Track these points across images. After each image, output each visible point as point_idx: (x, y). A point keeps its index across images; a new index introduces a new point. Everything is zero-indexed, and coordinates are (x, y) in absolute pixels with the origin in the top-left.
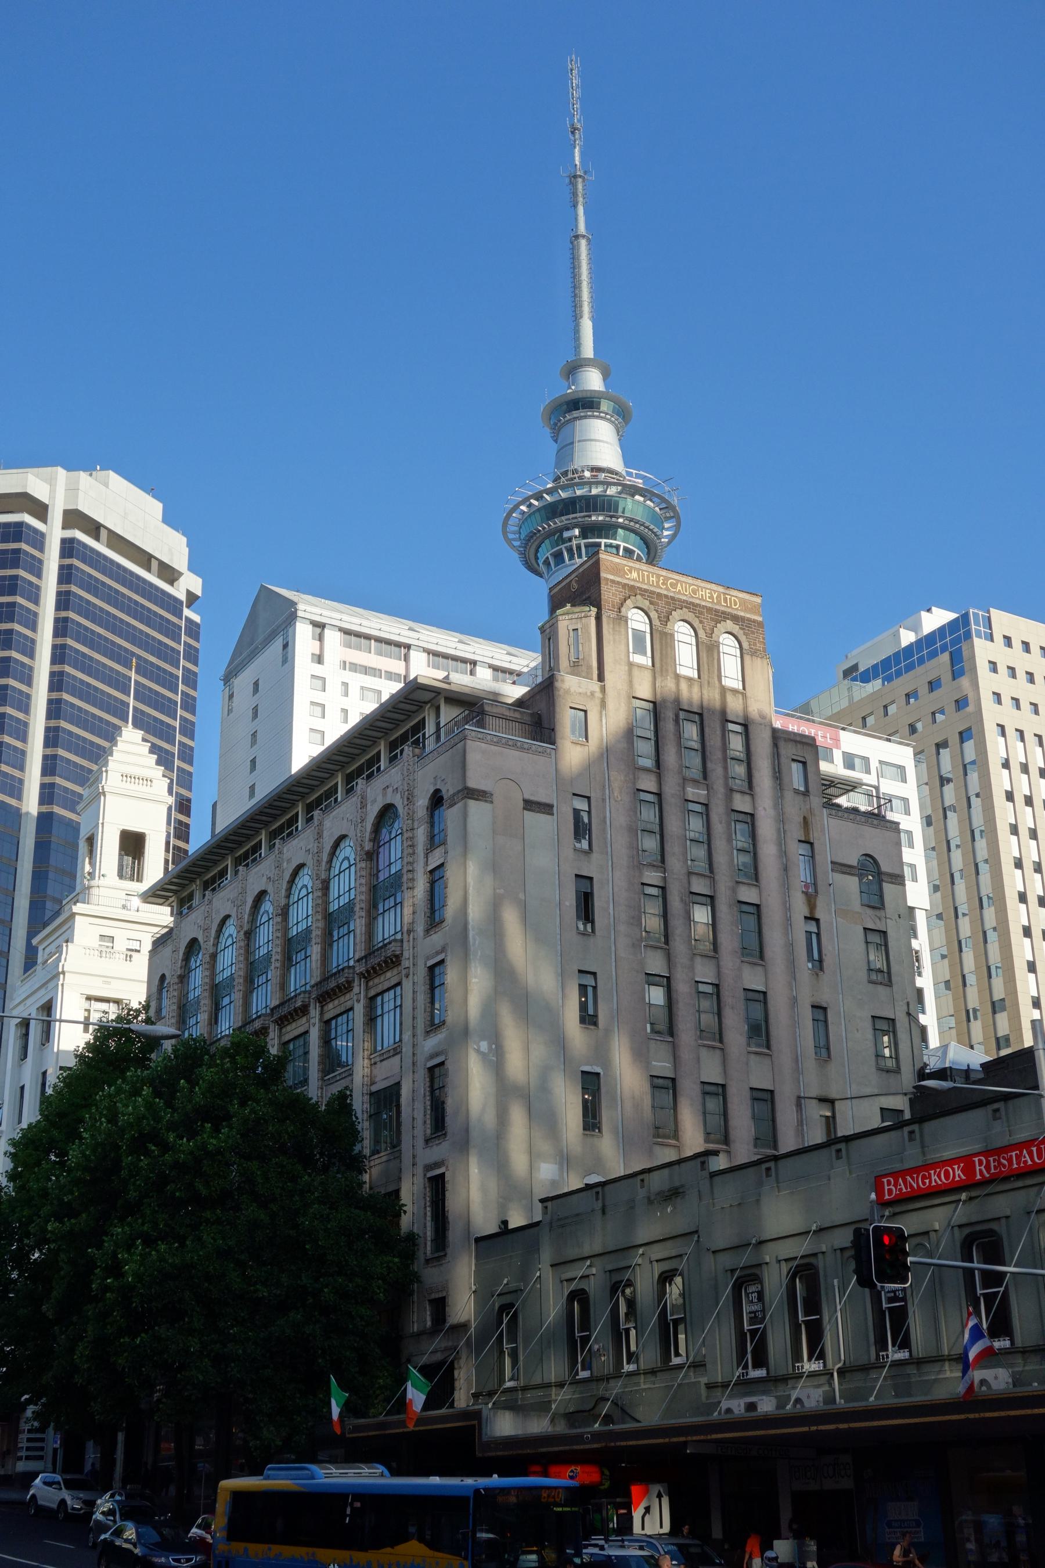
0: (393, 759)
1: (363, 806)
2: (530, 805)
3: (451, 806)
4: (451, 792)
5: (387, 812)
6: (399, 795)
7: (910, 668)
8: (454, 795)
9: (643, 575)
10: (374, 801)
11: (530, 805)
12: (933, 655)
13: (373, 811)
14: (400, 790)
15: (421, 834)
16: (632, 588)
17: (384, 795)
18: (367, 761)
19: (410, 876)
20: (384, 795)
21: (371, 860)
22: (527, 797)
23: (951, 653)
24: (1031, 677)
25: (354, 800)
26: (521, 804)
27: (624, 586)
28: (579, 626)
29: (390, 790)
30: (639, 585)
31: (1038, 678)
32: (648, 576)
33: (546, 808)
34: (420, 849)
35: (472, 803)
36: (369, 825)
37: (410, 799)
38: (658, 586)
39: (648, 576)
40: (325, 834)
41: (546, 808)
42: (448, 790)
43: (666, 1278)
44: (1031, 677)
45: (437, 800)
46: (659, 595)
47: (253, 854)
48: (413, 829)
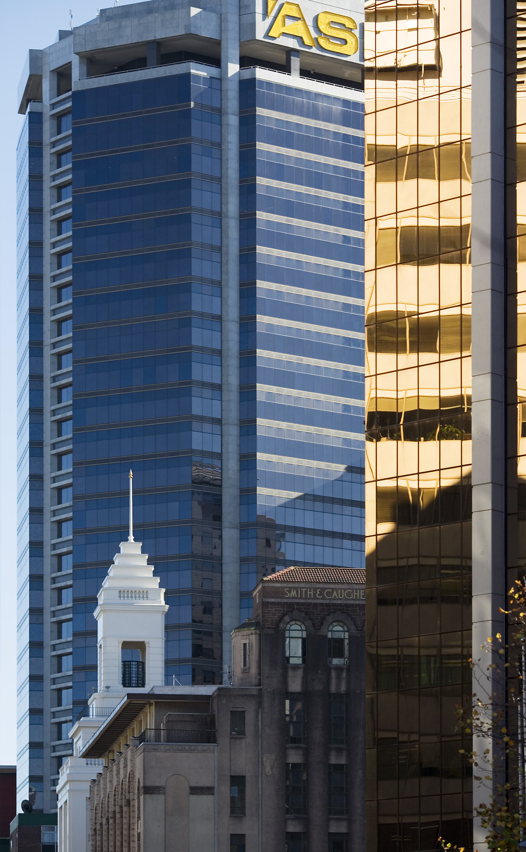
2: (195, 790)
9: (301, 592)
11: (195, 790)
22: (193, 784)
26: (188, 790)
28: (247, 641)
33: (208, 790)
38: (315, 598)
41: (208, 790)
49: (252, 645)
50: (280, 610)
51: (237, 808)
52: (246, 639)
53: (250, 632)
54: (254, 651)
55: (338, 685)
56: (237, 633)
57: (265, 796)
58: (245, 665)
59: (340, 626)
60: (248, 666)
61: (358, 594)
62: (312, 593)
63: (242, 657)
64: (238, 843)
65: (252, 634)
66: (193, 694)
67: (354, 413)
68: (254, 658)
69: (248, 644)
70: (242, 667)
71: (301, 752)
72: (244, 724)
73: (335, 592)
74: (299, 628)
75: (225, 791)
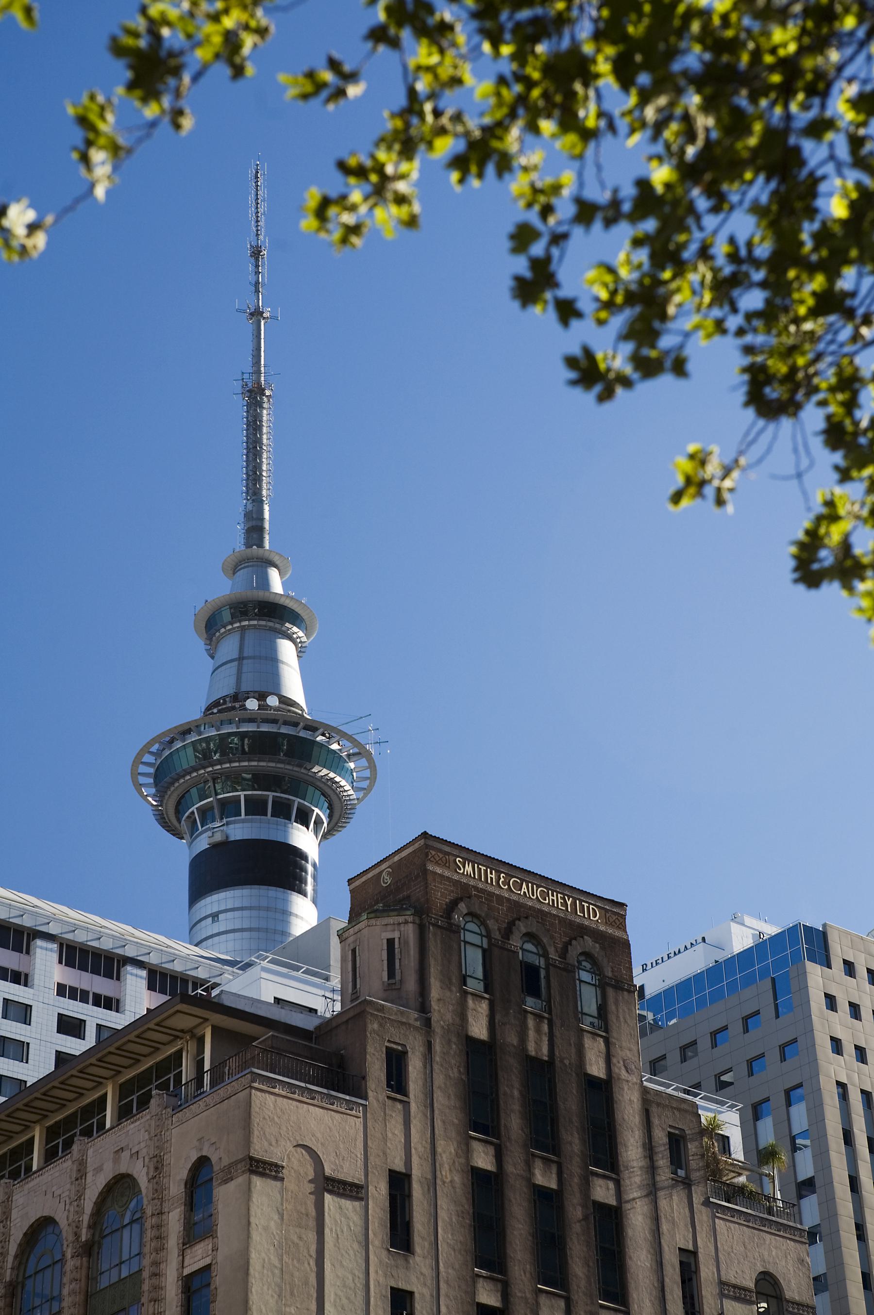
0: (50, 1156)
1: (81, 1174)
3: (226, 1181)
4: (226, 1162)
5: (121, 1185)
6: (140, 1163)
7: (716, 997)
8: (231, 1165)
10: (99, 1170)
12: (749, 981)
13: (95, 1185)
14: (143, 1153)
15: (175, 1220)
16: (465, 887)
17: (116, 1160)
18: (157, 1064)
19: (154, 1281)
20: (116, 1160)
21: (90, 1255)
23: (773, 979)
24: (855, 1010)
25: (65, 1166)
27: (457, 883)
28: (396, 935)
29: (126, 1155)
30: (472, 883)
31: (866, 1013)
32: (486, 871)
34: (173, 1242)
35: (258, 1182)
36: (88, 1206)
37: (158, 1166)
39: (486, 871)
40: (14, 1214)
41: (352, 1190)
42: (219, 1157)
43: (342, 1266)
44: (855, 1010)
45: (200, 1177)
46: (500, 898)
47: (83, 1121)
48: (161, 1213)
49: (407, 943)
50: (453, 891)
51: (400, 1236)
52: (394, 930)
53: (401, 919)
54: (412, 952)
55: (538, 1044)
56: (373, 922)
57: (441, 1220)
58: (391, 973)
59: (533, 944)
60: (398, 977)
61: (555, 898)
62: (493, 876)
63: (385, 962)
64: (401, 1302)
65: (406, 922)
66: (283, 1021)
67: (237, 800)
68: (412, 964)
69: (397, 941)
70: (385, 978)
71: (491, 1150)
72: (265, 1162)
73: (524, 885)
74: (477, 930)
75: (379, 1192)
